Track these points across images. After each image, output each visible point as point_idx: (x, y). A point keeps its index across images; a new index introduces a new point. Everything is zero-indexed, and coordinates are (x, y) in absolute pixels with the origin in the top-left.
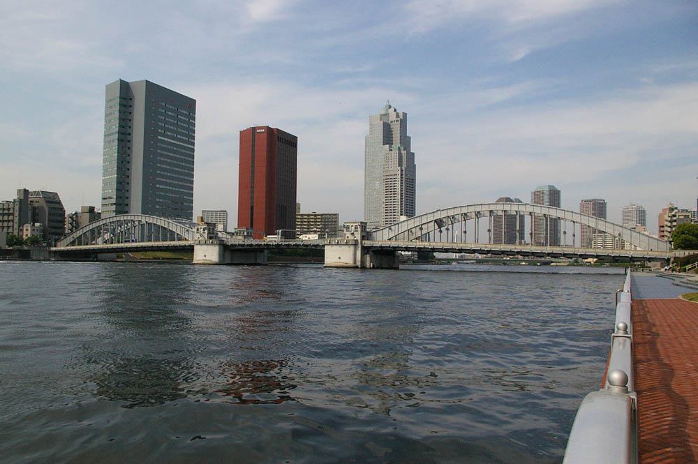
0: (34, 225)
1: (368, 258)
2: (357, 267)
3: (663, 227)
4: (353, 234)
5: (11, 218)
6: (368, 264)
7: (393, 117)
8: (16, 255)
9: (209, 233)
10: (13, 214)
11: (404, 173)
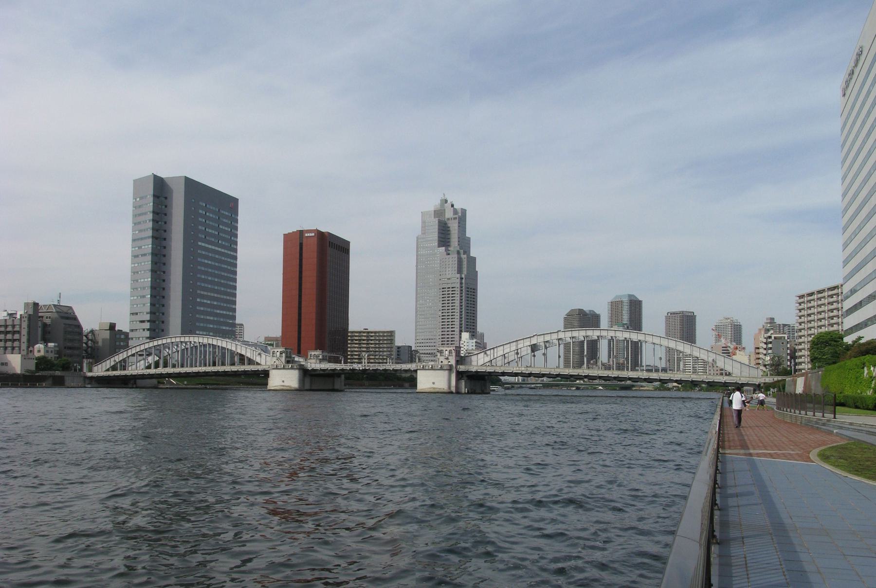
0: (46, 346)
1: (463, 383)
2: (451, 393)
3: (758, 348)
4: (447, 359)
5: (17, 336)
6: (463, 389)
7: (449, 214)
8: (50, 381)
9: (286, 357)
10: (19, 332)
11: (463, 281)
